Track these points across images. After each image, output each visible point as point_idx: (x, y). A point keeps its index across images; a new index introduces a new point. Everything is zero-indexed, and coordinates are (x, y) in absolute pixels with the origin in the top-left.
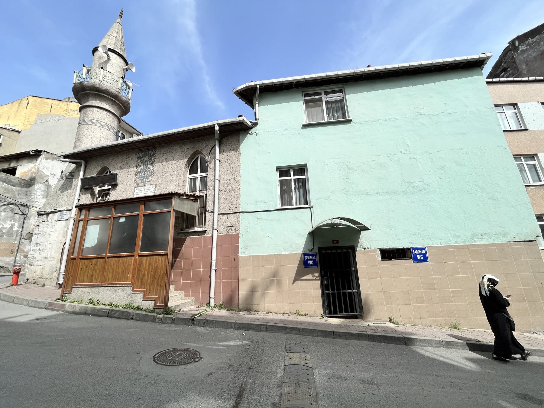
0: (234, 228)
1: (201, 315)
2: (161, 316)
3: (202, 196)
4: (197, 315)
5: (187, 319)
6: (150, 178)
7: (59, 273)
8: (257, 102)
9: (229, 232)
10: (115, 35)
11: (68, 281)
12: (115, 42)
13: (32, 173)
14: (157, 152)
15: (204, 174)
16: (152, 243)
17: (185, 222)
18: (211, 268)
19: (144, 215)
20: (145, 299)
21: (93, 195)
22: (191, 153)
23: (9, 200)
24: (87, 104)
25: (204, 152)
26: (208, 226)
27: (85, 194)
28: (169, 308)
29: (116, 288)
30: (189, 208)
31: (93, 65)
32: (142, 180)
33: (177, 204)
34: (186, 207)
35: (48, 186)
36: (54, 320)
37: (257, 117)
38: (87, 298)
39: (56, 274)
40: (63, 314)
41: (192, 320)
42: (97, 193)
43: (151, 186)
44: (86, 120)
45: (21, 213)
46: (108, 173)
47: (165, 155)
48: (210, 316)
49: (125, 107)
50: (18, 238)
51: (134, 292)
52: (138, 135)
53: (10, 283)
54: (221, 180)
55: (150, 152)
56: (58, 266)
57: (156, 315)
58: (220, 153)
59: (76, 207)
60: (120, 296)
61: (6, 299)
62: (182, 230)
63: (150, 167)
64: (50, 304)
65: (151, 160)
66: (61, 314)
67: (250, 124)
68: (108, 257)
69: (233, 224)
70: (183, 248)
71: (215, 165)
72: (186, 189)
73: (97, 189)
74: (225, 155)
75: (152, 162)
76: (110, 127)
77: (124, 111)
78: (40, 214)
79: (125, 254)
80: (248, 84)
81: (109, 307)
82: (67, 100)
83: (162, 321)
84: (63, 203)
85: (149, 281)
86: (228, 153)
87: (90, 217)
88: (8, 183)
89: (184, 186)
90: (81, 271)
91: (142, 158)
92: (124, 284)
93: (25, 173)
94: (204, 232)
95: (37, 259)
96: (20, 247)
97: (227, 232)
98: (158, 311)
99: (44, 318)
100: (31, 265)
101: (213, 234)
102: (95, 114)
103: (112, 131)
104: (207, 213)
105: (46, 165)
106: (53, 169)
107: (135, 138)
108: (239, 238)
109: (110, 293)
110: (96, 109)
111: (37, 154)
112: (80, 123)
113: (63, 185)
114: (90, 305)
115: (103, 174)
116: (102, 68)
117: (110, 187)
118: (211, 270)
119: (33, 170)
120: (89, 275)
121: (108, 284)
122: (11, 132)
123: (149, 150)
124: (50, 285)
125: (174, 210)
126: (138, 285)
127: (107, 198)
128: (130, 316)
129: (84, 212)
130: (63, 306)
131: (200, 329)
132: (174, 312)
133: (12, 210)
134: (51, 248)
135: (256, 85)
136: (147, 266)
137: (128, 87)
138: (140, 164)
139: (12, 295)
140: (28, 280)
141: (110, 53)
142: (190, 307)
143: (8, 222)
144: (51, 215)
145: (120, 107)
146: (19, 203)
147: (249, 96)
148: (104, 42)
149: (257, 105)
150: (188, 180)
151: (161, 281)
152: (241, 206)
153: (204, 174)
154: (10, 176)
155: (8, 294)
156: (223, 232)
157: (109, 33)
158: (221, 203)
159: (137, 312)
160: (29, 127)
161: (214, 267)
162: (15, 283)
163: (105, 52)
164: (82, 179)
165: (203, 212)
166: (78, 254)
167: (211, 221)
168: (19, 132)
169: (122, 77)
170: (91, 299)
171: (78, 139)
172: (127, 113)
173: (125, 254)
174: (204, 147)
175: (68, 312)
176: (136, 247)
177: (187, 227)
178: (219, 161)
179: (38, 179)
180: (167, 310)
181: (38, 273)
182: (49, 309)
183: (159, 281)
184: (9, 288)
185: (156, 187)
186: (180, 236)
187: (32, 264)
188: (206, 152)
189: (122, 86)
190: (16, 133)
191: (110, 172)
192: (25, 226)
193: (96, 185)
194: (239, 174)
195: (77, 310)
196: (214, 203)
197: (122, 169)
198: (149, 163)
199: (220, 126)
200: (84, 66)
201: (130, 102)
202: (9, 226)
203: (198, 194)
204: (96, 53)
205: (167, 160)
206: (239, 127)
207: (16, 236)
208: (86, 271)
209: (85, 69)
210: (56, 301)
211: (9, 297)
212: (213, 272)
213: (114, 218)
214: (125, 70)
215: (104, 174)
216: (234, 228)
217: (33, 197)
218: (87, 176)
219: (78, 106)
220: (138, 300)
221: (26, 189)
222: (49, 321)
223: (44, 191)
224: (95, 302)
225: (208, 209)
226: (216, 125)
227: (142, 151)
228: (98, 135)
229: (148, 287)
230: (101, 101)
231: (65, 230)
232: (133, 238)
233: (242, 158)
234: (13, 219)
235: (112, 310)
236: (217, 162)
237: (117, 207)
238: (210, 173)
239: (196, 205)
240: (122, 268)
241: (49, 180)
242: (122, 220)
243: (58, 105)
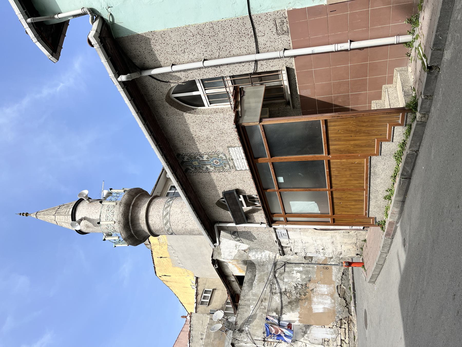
0: (278, 21)
1: (424, 56)
2: (418, 115)
3: (234, 82)
4: (423, 63)
5: (428, 77)
6: (220, 155)
7: (350, 229)
8: (56, 16)
9: (285, 29)
10: (53, 217)
11: (360, 222)
12: (61, 215)
13: (238, 264)
14: (183, 152)
15: (199, 85)
16: (311, 140)
17: (276, 101)
18: (347, 50)
19: (272, 156)
20: (391, 139)
21: (253, 211)
22: (173, 108)
23: (270, 277)
24: (147, 231)
25: (166, 92)
26: (280, 66)
27: (254, 218)
28: (408, 105)
29: (372, 174)
30: (255, 98)
31: (99, 231)
32: (225, 164)
33: (252, 119)
34: (253, 105)
35: (250, 249)
36: (408, 231)
37: (80, 11)
38: (383, 203)
39: (352, 233)
40: (401, 222)
41: (431, 69)
42: (250, 208)
43: (231, 152)
44: (166, 229)
45: (284, 267)
46: (224, 200)
47: (185, 142)
48: (427, 41)
49: (136, 194)
50: (311, 265)
51: (379, 153)
52: (166, 173)
53: (361, 269)
54: (203, 58)
55: (185, 159)
56: (342, 231)
57: (415, 122)
58: (160, 66)
59: (271, 226)
60: (384, 169)
61: (379, 270)
62: (288, 103)
63: (205, 158)
64: (388, 234)
65: (196, 157)
66: (401, 225)
67: (96, 23)
68: (331, 187)
69: (271, 24)
70: (316, 97)
71: (181, 71)
72: (227, 106)
73: (246, 208)
74: (161, 58)
75: (198, 156)
76: (166, 206)
77: (142, 194)
78: (284, 254)
79: (326, 170)
80: (35, 40)
81: (398, 179)
82: (149, 246)
83: (426, 114)
84: (267, 236)
85: (364, 138)
86: (156, 52)
87: (281, 211)
88: (253, 280)
89: (222, 111)
90: (348, 212)
91: (196, 168)
92: (367, 166)
93: (239, 269)
94: (289, 70)
95: (334, 250)
96: (321, 263)
97: (286, 33)
98: (409, 120)
99: (404, 241)
100: (341, 253)
101: (292, 57)
102: (156, 221)
103: (171, 202)
104: (259, 70)
105: (227, 254)
106: (230, 249)
107: (170, 175)
108: (295, 10)
109: (379, 180)
110: (150, 222)
111: (215, 262)
112: (172, 234)
113: (247, 239)
114: (393, 198)
115: (226, 205)
116: (99, 223)
117: (241, 196)
118: (351, 50)
119: (235, 263)
120: (353, 203)
121: (367, 183)
122: (199, 284)
123: (183, 162)
124: (365, 235)
125: (260, 121)
126: (371, 150)
127: (255, 197)
128: (413, 154)
129: (275, 218)
130: (390, 223)
131: (447, 55)
132: (415, 97)
133: (281, 274)
134: (321, 240)
135: (28, 24)
136: (342, 143)
137: (110, 194)
138: (204, 169)
139: (375, 266)
140: (357, 254)
141: (78, 217)
142: (409, 74)
143: (294, 275)
144: (283, 245)
145: (138, 199)
146: (273, 270)
147: (52, 34)
148: (71, 228)
149: (60, 16)
150: (213, 106)
151: (364, 122)
152: (239, 15)
153: (198, 85)
154: (245, 279)
155: (373, 269)
156: (287, 39)
157: (55, 223)
158: (238, 52)
159: (408, 146)
160: (190, 272)
161: (346, 46)
162: (362, 264)
163: (79, 224)
164: (237, 224)
165: (258, 77)
166: (329, 217)
167: (271, 63)
168: (197, 278)
169: (101, 202)
170: (385, 198)
171: (191, 233)
172: (143, 191)
173: (326, 170)
174: (159, 92)
175: (399, 218)
176: (316, 159)
177: (283, 96)
178: (173, 65)
179: (245, 258)
180: (411, 108)
181: (350, 247)
182: (393, 236)
183: (365, 124)
184: (366, 268)
185: (231, 147)
186: (298, 103)
187: (339, 253)
188: (165, 89)
189: (111, 201)
190: (199, 280)
191: (222, 198)
192: (297, 262)
193: (240, 210)
194: (186, 28)
195: (397, 210)
196: (240, 63)
197: (215, 187)
198: (201, 159)
199: (118, 73)
200: (105, 240)
201: (127, 189)
202: (299, 275)
203: (232, 89)
204: (84, 230)
205: (192, 139)
206: (108, 41)
207: (309, 267)
208: (348, 208)
209: (107, 239)
210: (384, 231)
211: (376, 267)
212: (355, 45)
213: (279, 188)
214: (90, 200)
215: (226, 204)
216: (278, 21)
217: (264, 260)
218: (232, 220)
219: (151, 238)
220: (390, 148)
221: (257, 266)
222: (408, 236)
223: (256, 252)
224: (388, 193)
225: (252, 71)
226: (119, 79)
227: (187, 170)
228: (180, 215)
229: (373, 137)
230: (138, 219)
231: (299, 230)
232: (304, 165)
233: (159, 28)
234: (291, 272)
235: (402, 174)
236: (175, 68)
237: (265, 186)
238: (197, 76)
239: (248, 89)
240: (346, 171)
241: (244, 249)
242: (281, 180)
243: (158, 252)
